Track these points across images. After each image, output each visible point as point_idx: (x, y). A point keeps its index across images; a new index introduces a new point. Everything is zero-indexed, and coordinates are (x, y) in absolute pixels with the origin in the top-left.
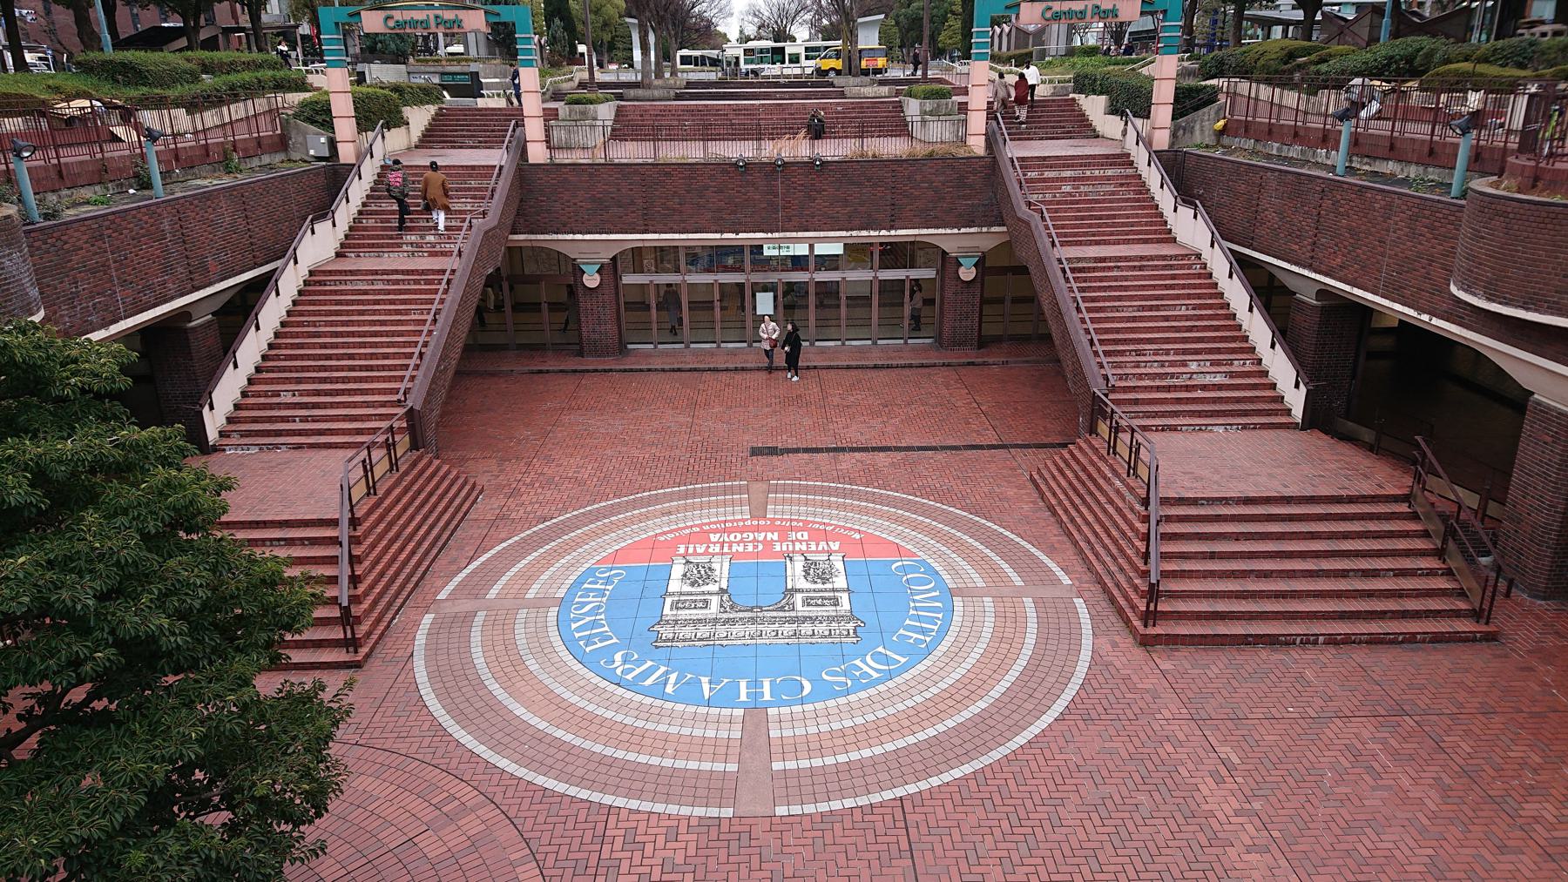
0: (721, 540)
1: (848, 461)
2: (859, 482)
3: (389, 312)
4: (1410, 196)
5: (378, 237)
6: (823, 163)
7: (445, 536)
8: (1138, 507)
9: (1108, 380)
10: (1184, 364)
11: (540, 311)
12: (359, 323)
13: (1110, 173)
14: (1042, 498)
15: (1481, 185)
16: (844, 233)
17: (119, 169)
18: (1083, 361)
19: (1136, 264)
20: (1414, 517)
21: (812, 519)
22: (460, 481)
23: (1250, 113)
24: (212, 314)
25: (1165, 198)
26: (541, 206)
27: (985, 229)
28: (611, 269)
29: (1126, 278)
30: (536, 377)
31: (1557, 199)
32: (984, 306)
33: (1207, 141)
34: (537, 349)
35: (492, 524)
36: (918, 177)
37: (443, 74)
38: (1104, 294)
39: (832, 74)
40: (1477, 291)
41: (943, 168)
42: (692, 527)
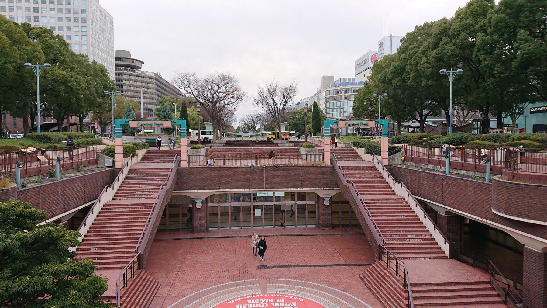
0: (252, 302)
1: (294, 270)
2: (299, 279)
3: (131, 219)
4: (473, 181)
5: (127, 193)
6: (279, 167)
7: (149, 303)
8: (402, 287)
9: (383, 240)
10: (406, 235)
11: (179, 217)
12: (120, 223)
13: (370, 172)
14: (365, 285)
15: (496, 178)
16: (285, 189)
17: (45, 171)
18: (374, 234)
19: (385, 201)
20: (493, 289)
21: (284, 293)
22: (154, 281)
23: (413, 155)
24: (68, 220)
25: (390, 180)
26: (184, 181)
27: (332, 189)
28: (205, 202)
29: (382, 206)
30: (177, 241)
31: (521, 183)
32: (333, 214)
33: (400, 163)
34: (177, 230)
35: (166, 298)
36: (309, 172)
37: (147, 139)
38: (376, 211)
39: (272, 139)
40: (502, 212)
41: (317, 169)
42: (240, 297)
